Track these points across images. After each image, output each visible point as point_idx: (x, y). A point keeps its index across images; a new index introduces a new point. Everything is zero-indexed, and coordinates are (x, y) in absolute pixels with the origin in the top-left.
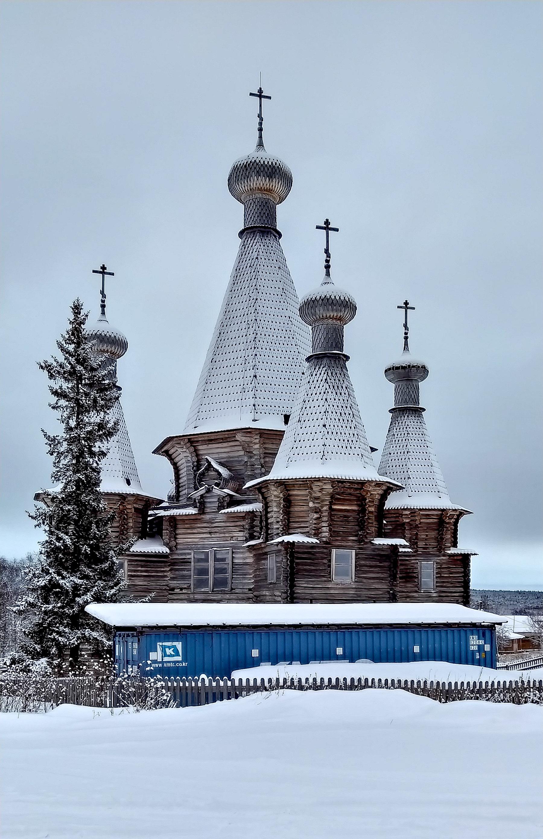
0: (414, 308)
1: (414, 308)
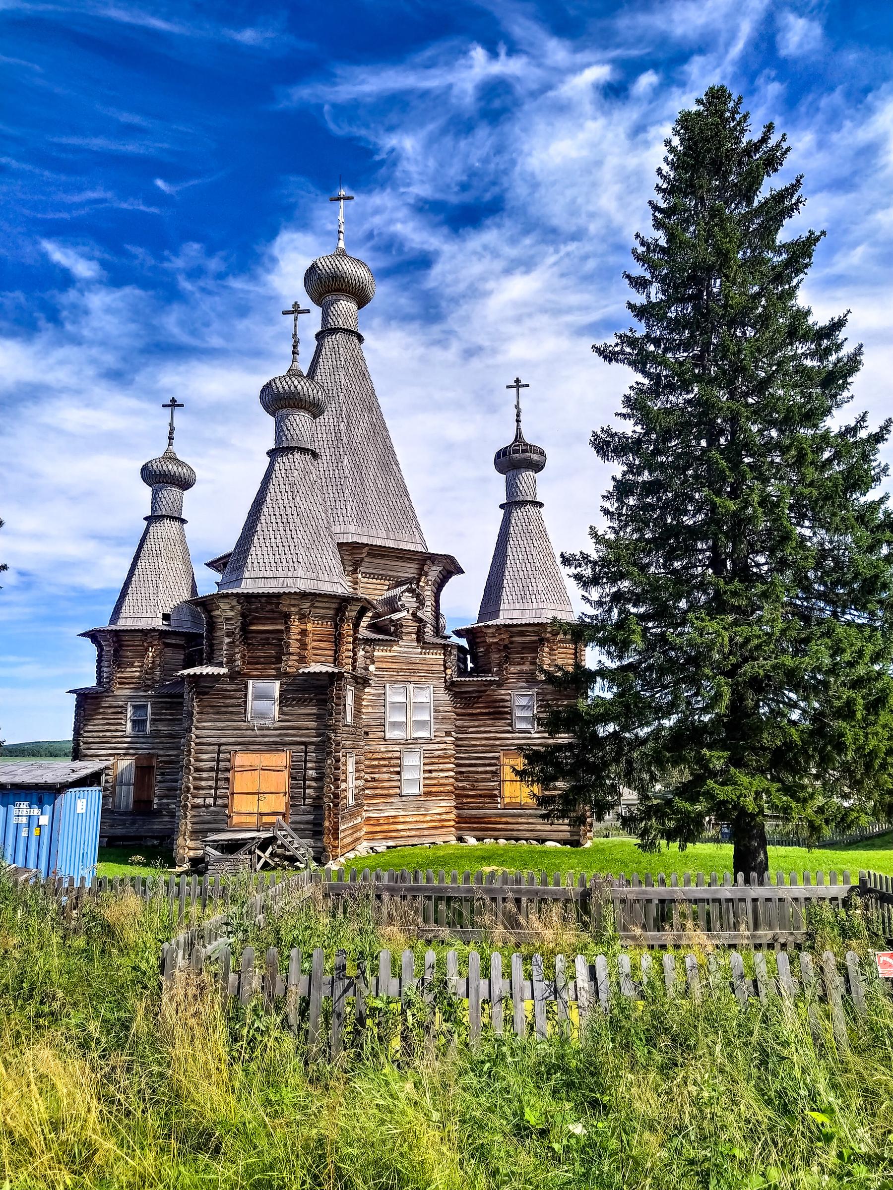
0: (527, 386)
1: (527, 386)
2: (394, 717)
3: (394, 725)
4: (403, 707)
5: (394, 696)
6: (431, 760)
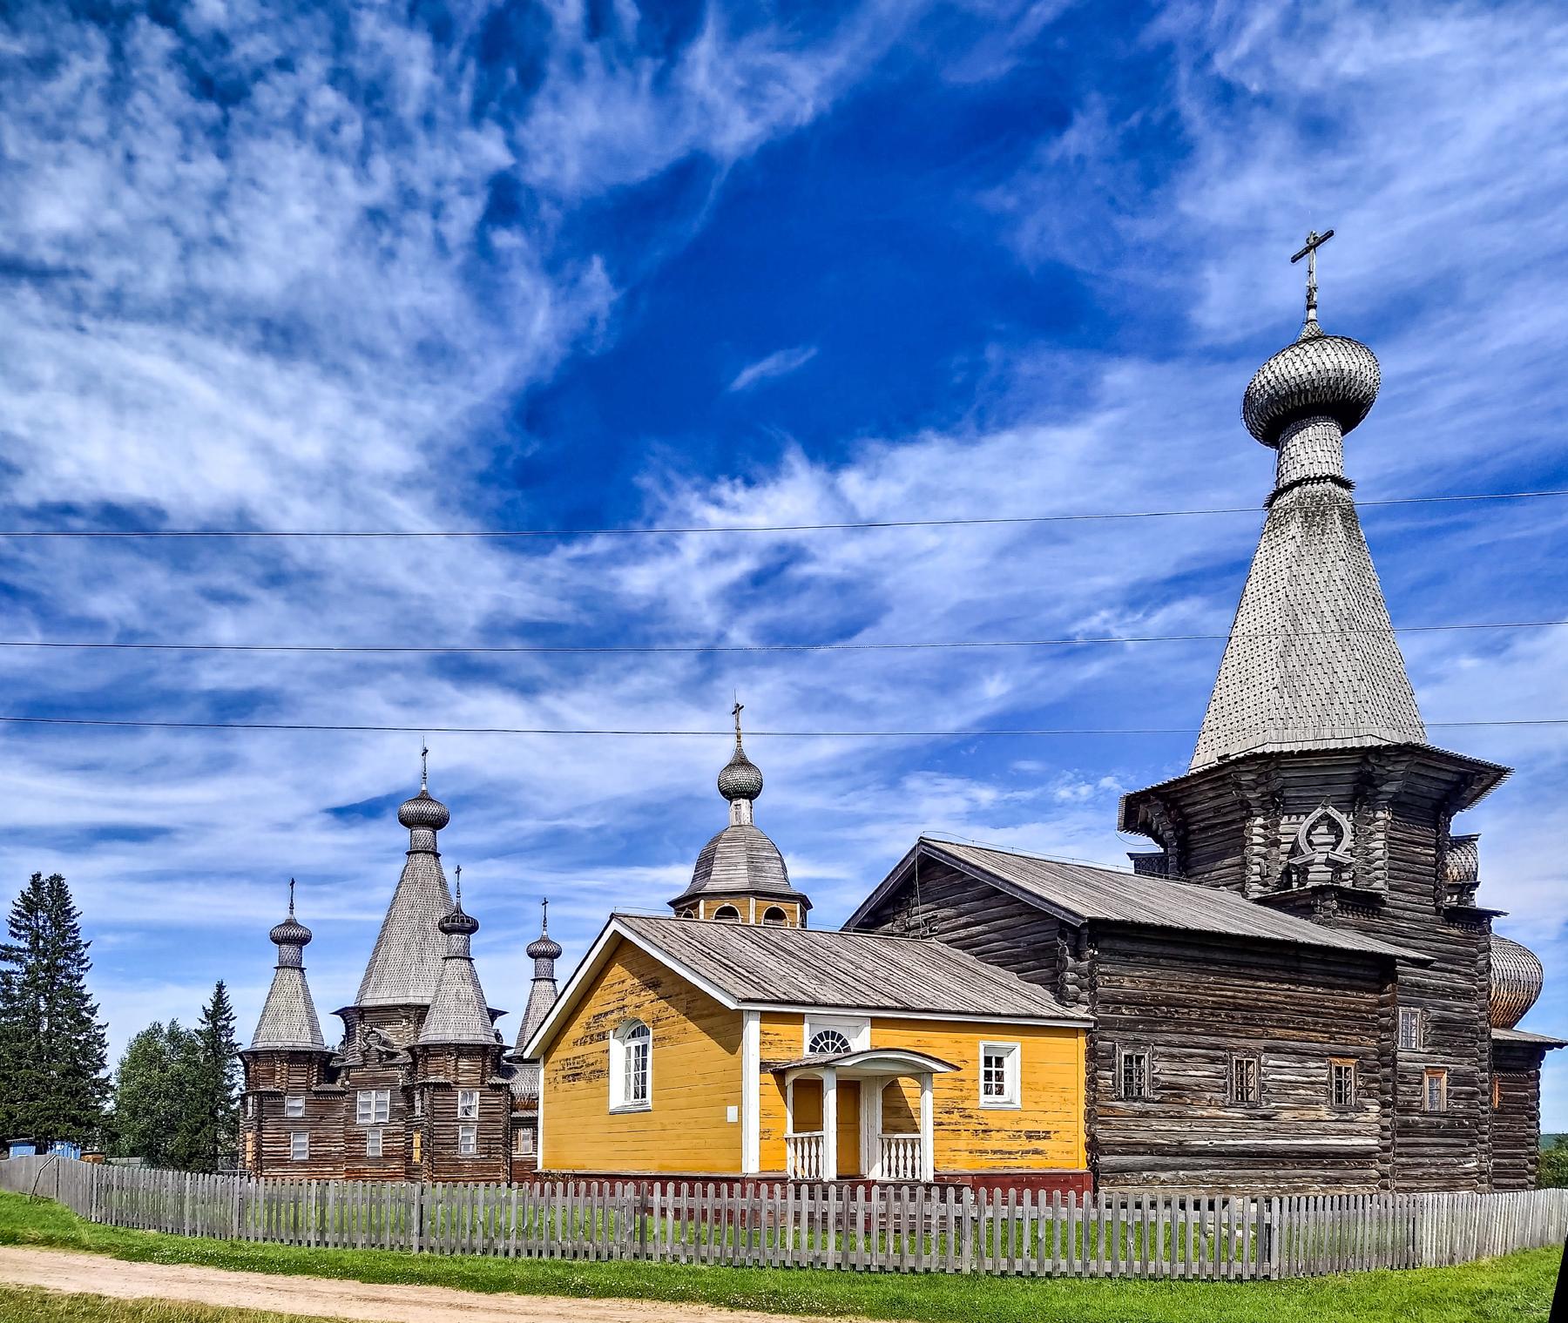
2: (360, 1110)
3: (363, 1116)
4: (368, 1105)
5: (361, 1098)
6: (387, 1135)
